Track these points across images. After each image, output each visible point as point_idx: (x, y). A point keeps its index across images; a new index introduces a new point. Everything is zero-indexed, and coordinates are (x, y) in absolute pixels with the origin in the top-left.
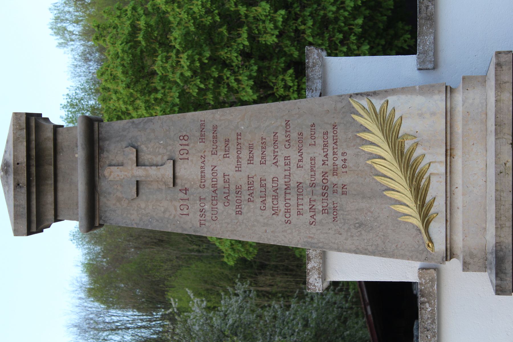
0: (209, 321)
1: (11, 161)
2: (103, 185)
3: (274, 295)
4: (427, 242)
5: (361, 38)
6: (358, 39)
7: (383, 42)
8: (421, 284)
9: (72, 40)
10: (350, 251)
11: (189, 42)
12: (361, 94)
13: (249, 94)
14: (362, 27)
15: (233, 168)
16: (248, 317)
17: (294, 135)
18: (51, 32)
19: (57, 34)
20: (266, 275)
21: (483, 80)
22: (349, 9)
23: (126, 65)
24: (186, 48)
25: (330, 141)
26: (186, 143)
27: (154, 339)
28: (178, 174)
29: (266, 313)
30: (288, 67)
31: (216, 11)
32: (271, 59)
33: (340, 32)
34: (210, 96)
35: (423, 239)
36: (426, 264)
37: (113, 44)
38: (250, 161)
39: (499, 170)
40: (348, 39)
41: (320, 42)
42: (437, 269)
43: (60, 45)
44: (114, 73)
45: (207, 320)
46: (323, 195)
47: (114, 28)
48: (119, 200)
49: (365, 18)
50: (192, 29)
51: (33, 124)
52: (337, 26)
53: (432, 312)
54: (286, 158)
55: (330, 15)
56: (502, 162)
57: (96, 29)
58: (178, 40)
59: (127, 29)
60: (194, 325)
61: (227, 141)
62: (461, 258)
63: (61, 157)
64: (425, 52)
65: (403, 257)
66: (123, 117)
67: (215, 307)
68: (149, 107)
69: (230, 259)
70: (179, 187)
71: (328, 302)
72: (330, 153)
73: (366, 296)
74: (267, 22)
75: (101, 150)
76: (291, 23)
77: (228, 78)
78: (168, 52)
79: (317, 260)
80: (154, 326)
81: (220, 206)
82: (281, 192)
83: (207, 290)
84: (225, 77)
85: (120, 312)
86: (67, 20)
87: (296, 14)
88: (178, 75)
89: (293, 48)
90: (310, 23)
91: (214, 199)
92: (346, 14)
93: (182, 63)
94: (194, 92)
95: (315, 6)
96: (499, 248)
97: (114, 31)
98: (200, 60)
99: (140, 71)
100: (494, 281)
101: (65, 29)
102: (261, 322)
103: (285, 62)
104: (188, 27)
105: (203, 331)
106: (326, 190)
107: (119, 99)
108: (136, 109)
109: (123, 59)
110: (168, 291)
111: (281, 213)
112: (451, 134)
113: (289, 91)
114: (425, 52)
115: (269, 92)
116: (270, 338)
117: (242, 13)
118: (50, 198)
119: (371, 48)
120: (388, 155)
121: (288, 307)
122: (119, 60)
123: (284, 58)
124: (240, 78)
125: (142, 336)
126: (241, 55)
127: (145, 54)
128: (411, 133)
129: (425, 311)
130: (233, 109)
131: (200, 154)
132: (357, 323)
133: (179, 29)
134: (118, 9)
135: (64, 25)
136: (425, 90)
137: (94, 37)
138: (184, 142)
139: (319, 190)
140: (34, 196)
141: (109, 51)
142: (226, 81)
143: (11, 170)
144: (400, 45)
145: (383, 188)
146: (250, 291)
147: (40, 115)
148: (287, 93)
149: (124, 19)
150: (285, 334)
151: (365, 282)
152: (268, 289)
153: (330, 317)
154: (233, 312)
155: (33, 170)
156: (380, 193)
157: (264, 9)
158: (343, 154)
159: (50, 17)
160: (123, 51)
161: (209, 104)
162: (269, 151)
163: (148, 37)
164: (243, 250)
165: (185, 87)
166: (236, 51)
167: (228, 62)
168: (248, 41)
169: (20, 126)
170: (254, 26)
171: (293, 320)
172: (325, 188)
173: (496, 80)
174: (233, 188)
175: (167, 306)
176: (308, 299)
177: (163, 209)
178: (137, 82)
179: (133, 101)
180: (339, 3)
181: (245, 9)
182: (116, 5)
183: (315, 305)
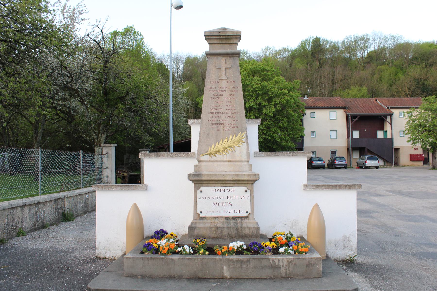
2: (220, 58)
3: (188, 113)
5: (265, 138)
10: (200, 131)
11: (263, 87)
12: (247, 135)
13: (248, 105)
17: (235, 115)
21: (251, 170)
24: (261, 86)
25: (233, 126)
28: (223, 80)
32: (258, 112)
34: (247, 93)
38: (227, 102)
46: (217, 124)
48: (215, 63)
50: (267, 88)
54: (228, 113)
55: (271, 129)
59: (267, 68)
61: (233, 95)
63: (228, 45)
65: (199, 147)
72: (230, 126)
75: (230, 57)
76: (269, 118)
81: (213, 93)
82: (217, 111)
90: (269, 123)
91: (216, 91)
114: (259, 154)
118: (216, 42)
136: (248, 154)
139: (218, 122)
140: (216, 37)
143: (224, 30)
149: (270, 68)
155: (224, 37)
159: (271, 46)
160: (261, 67)
162: (230, 108)
163: (265, 75)
172: (219, 124)
174: (219, 97)
175: (184, 81)
178: (251, 71)
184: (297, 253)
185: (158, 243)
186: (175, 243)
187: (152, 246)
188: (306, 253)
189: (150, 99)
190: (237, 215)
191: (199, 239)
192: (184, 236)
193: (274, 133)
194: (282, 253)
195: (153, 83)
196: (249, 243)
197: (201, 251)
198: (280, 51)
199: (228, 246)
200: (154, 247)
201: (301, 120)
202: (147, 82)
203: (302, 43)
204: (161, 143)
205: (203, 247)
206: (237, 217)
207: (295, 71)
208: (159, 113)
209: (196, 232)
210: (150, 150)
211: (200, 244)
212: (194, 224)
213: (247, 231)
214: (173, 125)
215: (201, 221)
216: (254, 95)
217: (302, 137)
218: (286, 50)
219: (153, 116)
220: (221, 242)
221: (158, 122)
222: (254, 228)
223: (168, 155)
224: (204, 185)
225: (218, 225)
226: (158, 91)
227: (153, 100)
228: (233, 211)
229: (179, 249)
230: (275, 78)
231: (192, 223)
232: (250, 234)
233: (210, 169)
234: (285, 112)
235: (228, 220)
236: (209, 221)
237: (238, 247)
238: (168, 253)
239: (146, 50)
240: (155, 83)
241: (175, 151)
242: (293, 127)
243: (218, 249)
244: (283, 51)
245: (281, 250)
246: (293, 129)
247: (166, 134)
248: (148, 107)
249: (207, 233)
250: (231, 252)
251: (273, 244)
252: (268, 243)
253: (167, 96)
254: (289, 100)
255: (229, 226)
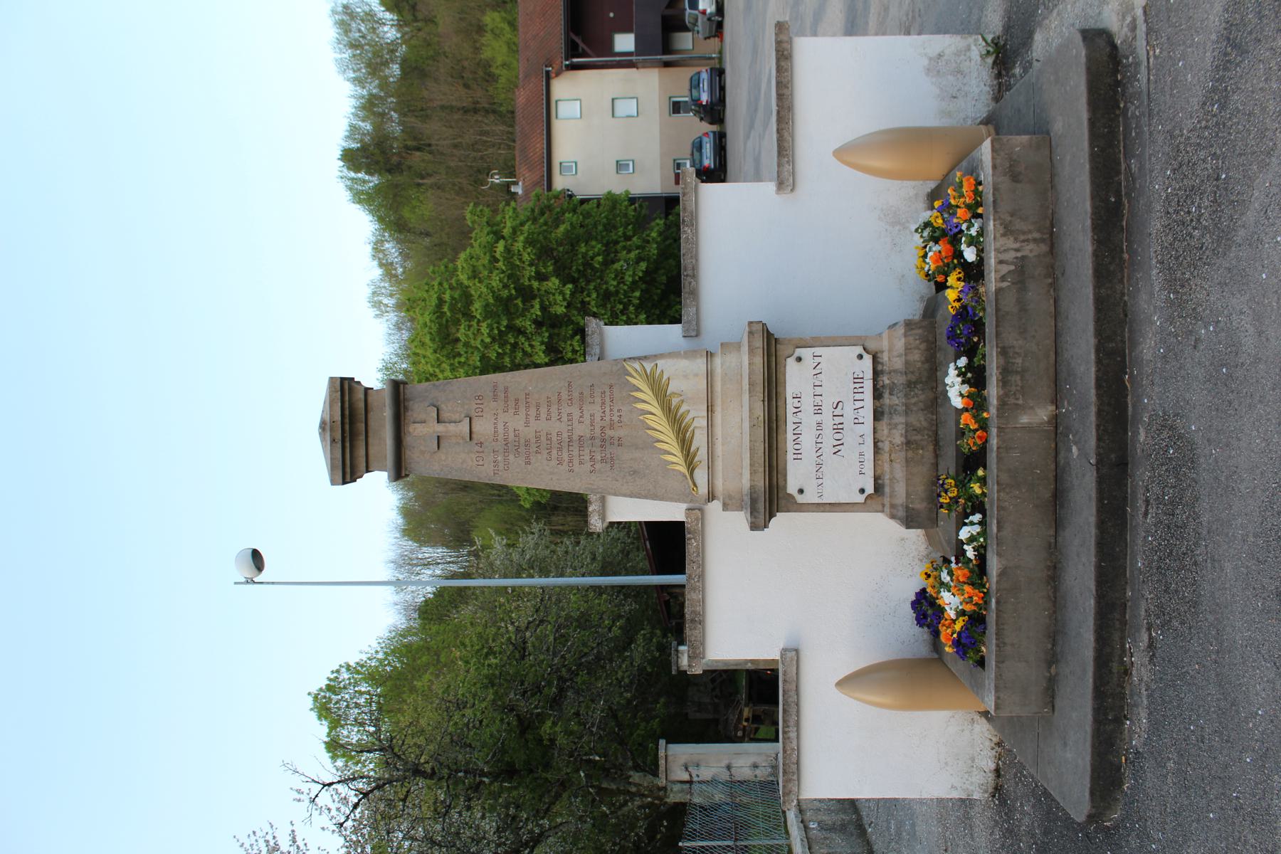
1: (328, 419)
2: (408, 440)
3: (566, 532)
6: (636, 309)
7: (657, 312)
10: (625, 495)
11: (488, 313)
13: (541, 357)
14: (639, 298)
19: (374, 306)
21: (738, 346)
24: (485, 318)
25: (608, 400)
33: (620, 303)
34: (507, 360)
36: (691, 505)
38: (537, 418)
43: (377, 316)
48: (423, 453)
50: (491, 301)
51: (346, 387)
53: (697, 547)
54: (569, 415)
55: (612, 289)
59: (434, 301)
61: (517, 400)
63: (371, 415)
64: (689, 322)
65: (671, 500)
70: (475, 441)
72: (607, 409)
75: (406, 409)
81: (511, 457)
82: (565, 445)
90: (594, 295)
91: (506, 451)
94: (493, 356)
101: (381, 302)
108: (442, 371)
114: (689, 322)
118: (362, 452)
120: (658, 411)
136: (690, 354)
139: (598, 442)
143: (328, 427)
149: (432, 293)
155: (347, 427)
156: (651, 445)
159: (369, 291)
162: (554, 409)
172: (603, 440)
174: (522, 441)
175: (472, 543)
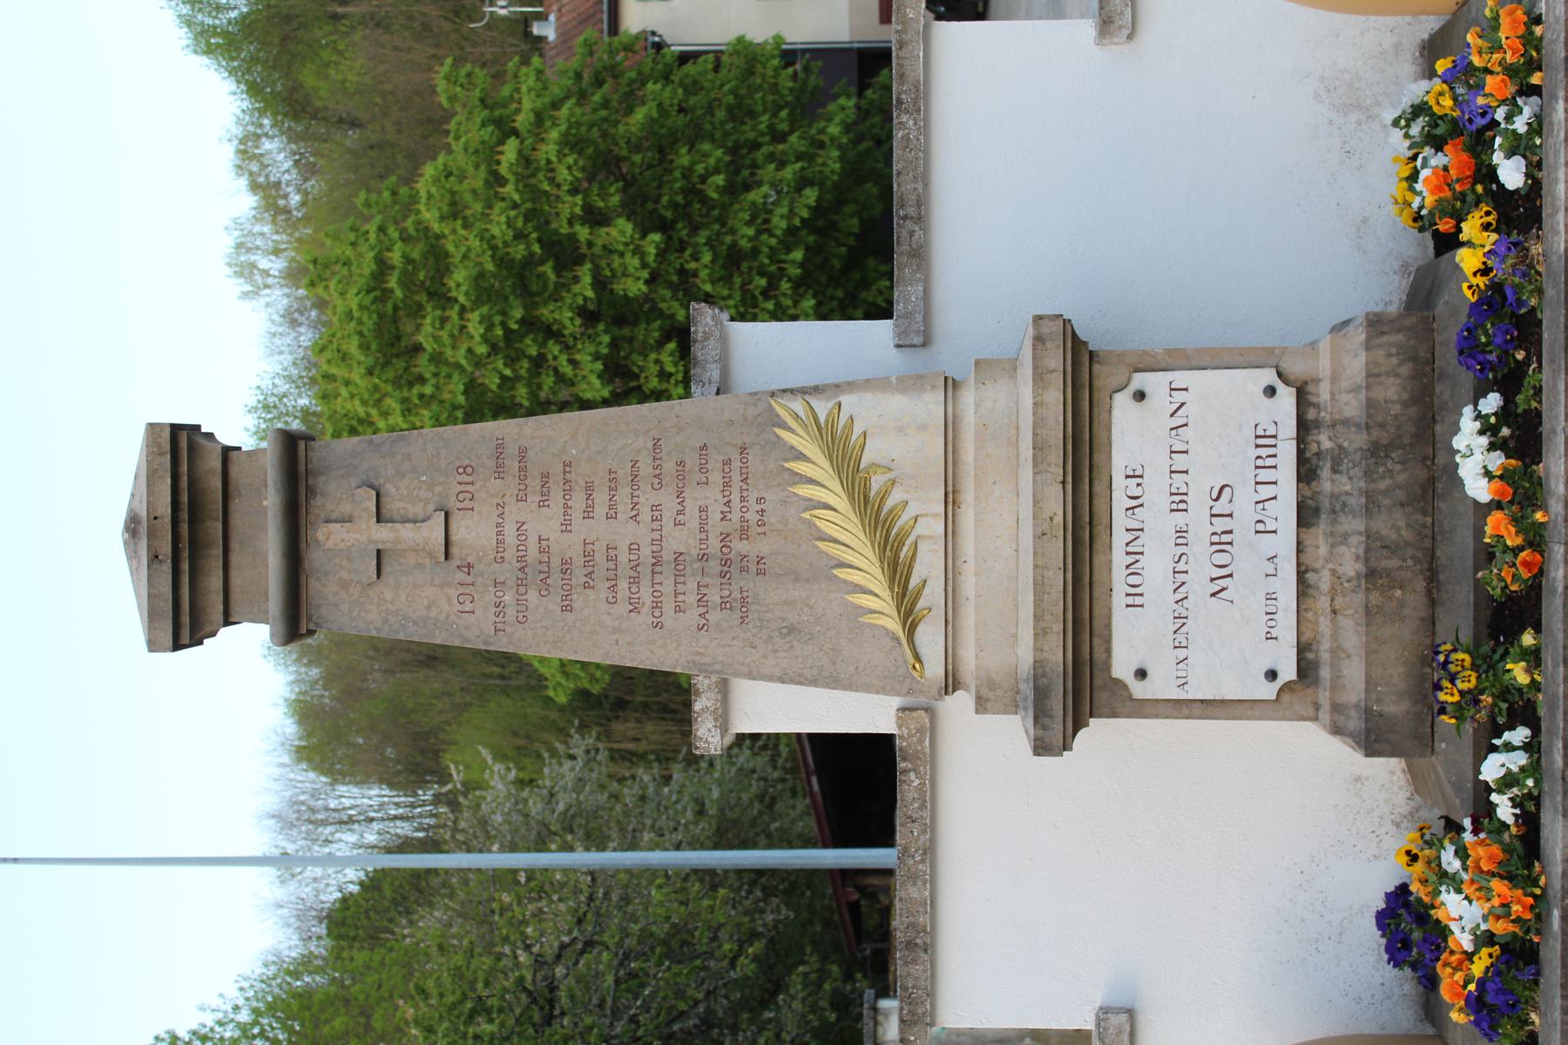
0: (521, 806)
1: (144, 514)
2: (314, 558)
3: (642, 757)
4: (912, 661)
5: (800, 285)
7: (840, 294)
8: (901, 737)
9: (267, 286)
10: (770, 678)
11: (483, 292)
12: (792, 391)
13: (594, 387)
14: (802, 265)
15: (557, 527)
16: (593, 798)
17: (669, 466)
18: (230, 271)
19: (239, 274)
20: (626, 721)
21: (1012, 366)
22: (779, 232)
23: (366, 333)
24: (477, 303)
25: (736, 477)
26: (470, 479)
27: (419, 840)
28: (454, 537)
29: (626, 791)
30: (666, 338)
31: (534, 235)
32: (635, 323)
33: (762, 274)
34: (522, 392)
35: (903, 655)
37: (343, 294)
38: (588, 513)
39: (1039, 530)
40: (777, 288)
41: (725, 292)
42: (930, 711)
43: (245, 295)
44: (344, 347)
45: (517, 803)
46: (722, 575)
47: (344, 264)
48: (345, 585)
49: (807, 249)
50: (490, 267)
51: (184, 444)
52: (756, 264)
55: (744, 244)
56: (1046, 515)
57: (311, 266)
58: (464, 288)
59: (368, 266)
60: (494, 813)
61: (545, 476)
62: (973, 690)
63: (236, 506)
64: (908, 316)
65: (867, 688)
66: (360, 429)
67: (532, 781)
68: (409, 410)
69: (560, 691)
70: (455, 562)
71: (741, 769)
72: (735, 498)
73: (810, 759)
74: (628, 255)
75: (311, 492)
77: (555, 358)
78: (444, 309)
79: (712, 695)
80: (421, 816)
81: (533, 596)
82: (645, 571)
83: (518, 748)
84: (550, 357)
85: (355, 790)
86: (258, 248)
87: (681, 241)
88: (463, 351)
89: (676, 304)
90: (707, 257)
91: (521, 583)
92: (773, 241)
93: (471, 329)
94: (493, 382)
95: (716, 227)
96: (1040, 671)
97: (345, 271)
98: (503, 324)
99: (392, 345)
100: (1032, 731)
101: (253, 266)
102: (618, 808)
103: (661, 329)
104: (481, 264)
105: (510, 823)
106: (728, 566)
107: (352, 396)
108: (385, 414)
109: (360, 322)
110: (444, 751)
111: (646, 610)
112: (955, 464)
113: (668, 381)
114: (908, 316)
115: (632, 384)
116: (634, 837)
117: (582, 239)
118: (216, 582)
119: (819, 305)
120: (841, 502)
121: (667, 779)
122: (353, 324)
123: (659, 322)
124: (578, 357)
125: (397, 835)
126: (579, 315)
127: (401, 313)
128: (883, 462)
129: (909, 787)
130: (566, 415)
131: (495, 501)
132: (794, 807)
133: (466, 268)
134: (353, 229)
135: (253, 258)
136: (909, 383)
137: (305, 281)
138: (465, 478)
139: (714, 566)
140: (185, 579)
141: (335, 307)
142: (551, 362)
143: (143, 529)
144: (870, 299)
145: (833, 563)
146: (597, 750)
147: (198, 427)
148: (664, 386)
149: (363, 248)
150: (661, 829)
151: (809, 735)
152: (631, 746)
153: (745, 797)
154: (565, 789)
156: (826, 572)
157: (623, 232)
158: (759, 500)
159: (228, 241)
160: (361, 307)
161: (521, 405)
162: (623, 493)
163: (407, 281)
164: (582, 675)
165: (477, 374)
166: (571, 308)
167: (555, 328)
168: (594, 289)
169: (160, 447)
170: (603, 263)
171: (677, 802)
172: (726, 562)
173: (1035, 367)
175: (444, 778)
176: (704, 765)
177: (425, 602)
178: (387, 364)
179: (379, 400)
180: (759, 221)
181: (587, 231)
182: (348, 223)
183: (716, 775)
184: (1536, 79)
185: (1468, 946)
186: (1468, 837)
187: (1490, 986)
188: (1538, 20)
189: (553, 988)
190: (1287, 452)
191: (1438, 687)
192: (1417, 779)
193: (765, 228)
194: (1534, 169)
195: (457, 974)
196: (1466, 378)
197: (1519, 673)
198: (255, 187)
199: (1482, 510)
200: (1494, 970)
201: (685, 58)
202: (454, 1006)
203: (209, 51)
204: (827, 924)
205: (1487, 665)
206: (1300, 453)
207: (384, 95)
208: (645, 934)
209: (1396, 707)
210: (869, 994)
211: (1468, 682)
212: (1341, 720)
213: (1391, 390)
214: (716, 847)
215: (1325, 673)
216: (533, 351)
217: (789, 56)
218: (247, 152)
219: (662, 975)
220: (1458, 551)
221: (701, 938)
222: (1368, 347)
223: (913, 877)
224: (1099, 655)
225: (1350, 567)
226: (506, 939)
227: (559, 971)
228: (1264, 475)
229: (1505, 811)
230: (430, 216)
231: (1337, 730)
232: (1405, 370)
233: (1005, 621)
234: (638, 158)
235: (1317, 511)
236: (1324, 625)
237: (1492, 447)
238: (1535, 883)
239: (244, 1016)
240: (458, 959)
241: (883, 835)
242: (730, 109)
243: (1507, 573)
244: (255, 167)
245: (1511, 174)
246: (740, 112)
247: (768, 892)
248: (601, 1005)
249: (1401, 637)
250: (1522, 488)
251: (1471, 228)
252: (1469, 260)
253: (539, 884)
254: (565, 135)
255: (1357, 501)
